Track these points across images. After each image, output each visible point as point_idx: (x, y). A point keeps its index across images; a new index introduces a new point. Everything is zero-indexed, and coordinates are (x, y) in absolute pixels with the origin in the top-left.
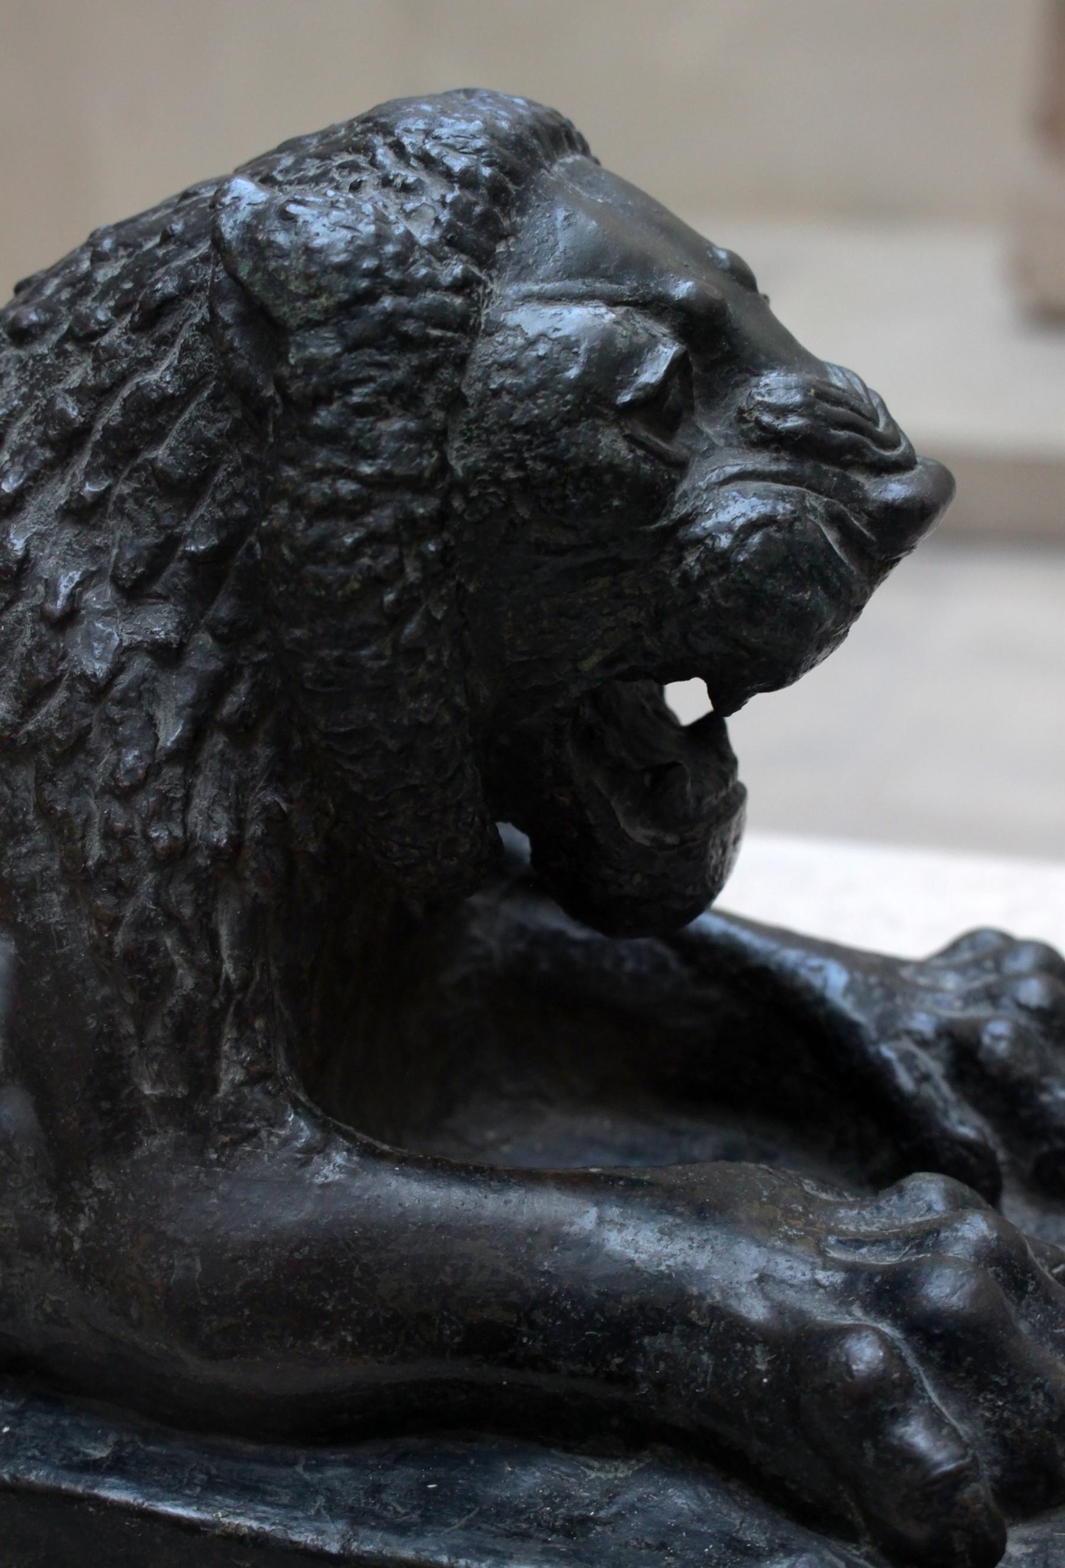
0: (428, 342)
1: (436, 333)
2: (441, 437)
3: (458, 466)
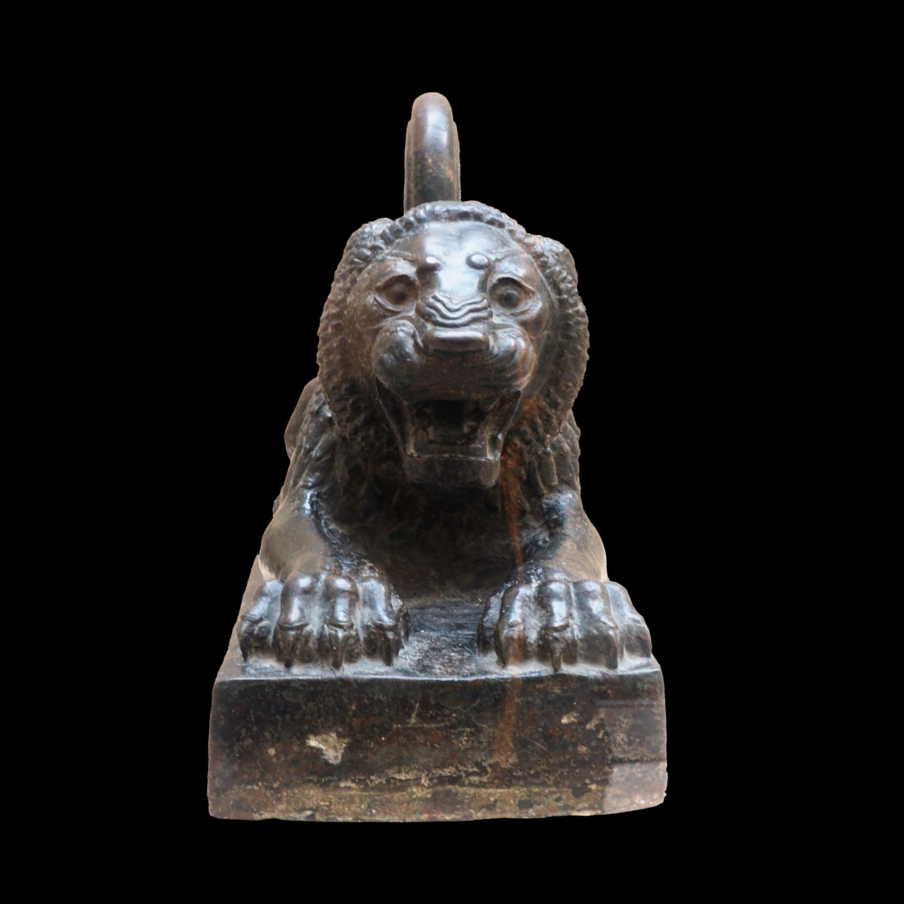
1: (356, 260)
2: (348, 291)
3: (348, 300)
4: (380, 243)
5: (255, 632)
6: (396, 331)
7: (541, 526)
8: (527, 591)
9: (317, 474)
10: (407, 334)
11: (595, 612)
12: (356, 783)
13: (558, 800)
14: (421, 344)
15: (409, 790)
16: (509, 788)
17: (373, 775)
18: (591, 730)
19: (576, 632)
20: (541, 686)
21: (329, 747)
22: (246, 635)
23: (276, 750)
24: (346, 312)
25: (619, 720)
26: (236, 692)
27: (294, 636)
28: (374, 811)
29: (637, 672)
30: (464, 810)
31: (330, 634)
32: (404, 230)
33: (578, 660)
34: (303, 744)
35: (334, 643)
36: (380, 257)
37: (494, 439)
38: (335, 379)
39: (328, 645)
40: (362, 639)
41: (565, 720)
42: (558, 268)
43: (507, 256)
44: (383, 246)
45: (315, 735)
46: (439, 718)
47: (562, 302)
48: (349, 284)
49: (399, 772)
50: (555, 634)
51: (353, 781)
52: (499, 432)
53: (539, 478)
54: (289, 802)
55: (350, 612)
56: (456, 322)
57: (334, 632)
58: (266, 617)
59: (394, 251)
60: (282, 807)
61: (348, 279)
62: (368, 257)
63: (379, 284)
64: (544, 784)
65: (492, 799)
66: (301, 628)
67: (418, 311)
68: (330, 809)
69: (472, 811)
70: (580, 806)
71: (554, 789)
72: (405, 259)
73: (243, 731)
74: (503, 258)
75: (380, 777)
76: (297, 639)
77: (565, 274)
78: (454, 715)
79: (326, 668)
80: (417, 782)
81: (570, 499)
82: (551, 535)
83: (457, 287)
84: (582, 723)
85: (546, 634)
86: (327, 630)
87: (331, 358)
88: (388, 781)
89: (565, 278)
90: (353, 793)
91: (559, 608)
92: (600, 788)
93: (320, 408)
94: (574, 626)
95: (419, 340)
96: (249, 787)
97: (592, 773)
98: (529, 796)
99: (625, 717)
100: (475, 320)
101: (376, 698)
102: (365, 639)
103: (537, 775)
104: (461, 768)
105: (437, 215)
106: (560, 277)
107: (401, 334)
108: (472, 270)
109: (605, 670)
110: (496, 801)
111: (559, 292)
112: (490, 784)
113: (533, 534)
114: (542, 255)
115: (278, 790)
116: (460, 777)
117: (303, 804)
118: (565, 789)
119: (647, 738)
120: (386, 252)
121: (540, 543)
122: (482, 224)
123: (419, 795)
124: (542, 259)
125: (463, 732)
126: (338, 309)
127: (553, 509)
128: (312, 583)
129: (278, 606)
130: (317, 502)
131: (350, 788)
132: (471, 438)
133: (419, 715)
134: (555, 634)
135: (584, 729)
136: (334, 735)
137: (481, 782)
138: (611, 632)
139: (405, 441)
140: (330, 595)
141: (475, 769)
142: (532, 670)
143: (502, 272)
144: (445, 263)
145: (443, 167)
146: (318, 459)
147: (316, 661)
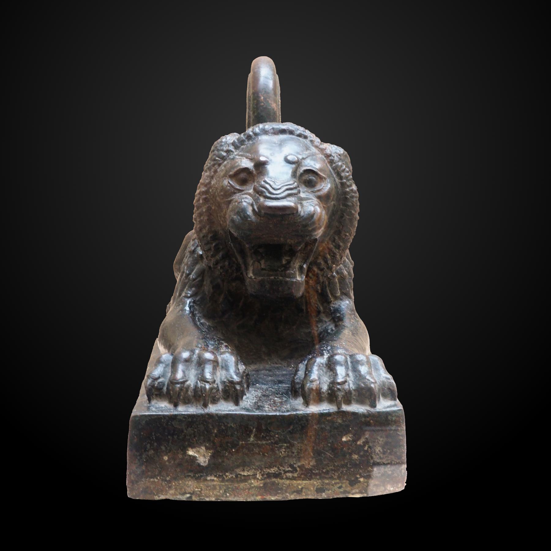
0: (215, 160)
1: (217, 158)
2: (212, 177)
3: (212, 183)
4: (231, 148)
5: (156, 385)
6: (242, 202)
7: (330, 321)
8: (321, 360)
9: (193, 289)
10: (248, 203)
11: (362, 373)
12: (217, 477)
13: (340, 488)
14: (256, 209)
15: (249, 481)
16: (310, 480)
17: (227, 472)
18: (360, 445)
19: (351, 385)
20: (330, 418)
21: (200, 455)
22: (150, 387)
23: (168, 457)
24: (211, 190)
25: (377, 439)
26: (144, 422)
27: (179, 388)
28: (228, 494)
29: (388, 410)
30: (283, 494)
31: (201, 387)
32: (246, 140)
33: (352, 402)
34: (185, 453)
35: (203, 392)
36: (231, 157)
37: (301, 268)
38: (204, 231)
39: (200, 393)
40: (220, 389)
41: (344, 439)
42: (340, 164)
43: (309, 156)
44: (233, 150)
45: (192, 448)
46: (267, 438)
47: (343, 184)
48: (213, 173)
49: (243, 470)
50: (338, 387)
51: (215, 476)
52: (304, 263)
53: (328, 291)
54: (176, 489)
55: (213, 373)
56: (278, 196)
57: (203, 385)
58: (162, 376)
59: (240, 153)
60: (172, 492)
61: (212, 170)
62: (224, 156)
63: (231, 173)
64: (332, 478)
65: (300, 487)
66: (184, 383)
67: (255, 189)
68: (201, 493)
69: (288, 494)
70: (354, 491)
71: (338, 481)
72: (247, 158)
73: (148, 446)
74: (307, 157)
75: (231, 474)
76: (181, 389)
77: (344, 167)
78: (277, 436)
79: (199, 407)
80: (254, 476)
81: (347, 304)
82: (336, 326)
83: (278, 175)
84: (355, 441)
85: (333, 386)
86: (199, 384)
87: (202, 218)
88: (237, 476)
89: (345, 169)
90: (215, 483)
91: (341, 371)
92: (366, 480)
93: (195, 249)
94: (350, 382)
95: (255, 207)
96: (152, 480)
97: (361, 471)
98: (322, 485)
99: (381, 437)
100: (289, 195)
101: (229, 425)
102: (222, 389)
103: (327, 472)
104: (281, 468)
105: (267, 131)
106: (342, 169)
107: (245, 204)
108: (288, 164)
109: (368, 408)
110: (302, 488)
111: (341, 178)
112: (299, 478)
113: (325, 326)
114: (331, 155)
115: (169, 482)
116: (280, 474)
117: (185, 490)
118: (344, 481)
119: (394, 450)
120: (235, 153)
121: (329, 331)
122: (294, 136)
123: (256, 485)
124: (330, 158)
125: (282, 446)
126: (206, 189)
127: (337, 310)
128: (190, 356)
129: (169, 370)
130: (193, 306)
131: (213, 480)
132: (287, 267)
133: (255, 436)
134: (338, 387)
135: (356, 444)
136: (203, 448)
137: (293, 476)
138: (372, 386)
139: (247, 269)
140: (201, 363)
141: (290, 469)
142: (325, 408)
143: (306, 166)
144: (271, 160)
145: (270, 102)
146: (194, 280)
147: (193, 403)
